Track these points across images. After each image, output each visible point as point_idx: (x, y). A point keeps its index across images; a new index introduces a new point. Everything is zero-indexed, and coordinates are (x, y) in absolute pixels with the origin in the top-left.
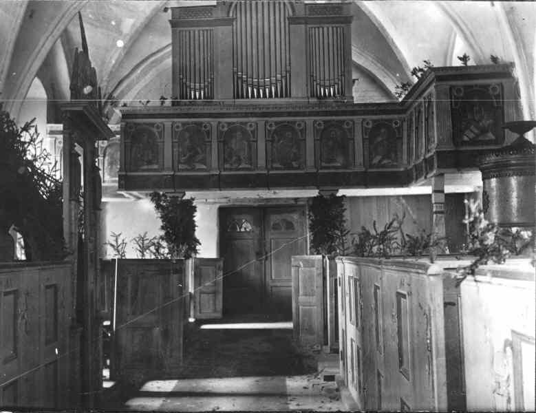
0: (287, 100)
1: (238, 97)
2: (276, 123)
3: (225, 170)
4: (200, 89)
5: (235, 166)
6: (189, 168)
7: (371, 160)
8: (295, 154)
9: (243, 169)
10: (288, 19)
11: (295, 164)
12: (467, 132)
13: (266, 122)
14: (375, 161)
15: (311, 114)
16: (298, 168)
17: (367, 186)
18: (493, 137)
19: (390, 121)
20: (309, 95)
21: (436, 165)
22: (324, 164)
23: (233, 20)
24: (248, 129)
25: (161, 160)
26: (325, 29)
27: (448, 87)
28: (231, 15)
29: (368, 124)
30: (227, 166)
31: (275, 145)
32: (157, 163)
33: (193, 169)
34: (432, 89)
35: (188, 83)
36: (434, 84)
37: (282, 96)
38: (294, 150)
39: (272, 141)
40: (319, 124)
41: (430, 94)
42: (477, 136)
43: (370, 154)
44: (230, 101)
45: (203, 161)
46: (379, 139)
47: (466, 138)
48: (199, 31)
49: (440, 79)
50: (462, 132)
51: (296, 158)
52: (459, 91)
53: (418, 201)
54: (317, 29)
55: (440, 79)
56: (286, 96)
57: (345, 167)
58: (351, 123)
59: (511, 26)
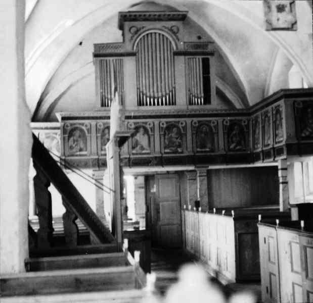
0: (174, 106)
3: (133, 154)
5: (139, 151)
8: (179, 143)
11: (179, 150)
12: (305, 131)
13: (128, 123)
14: (232, 146)
15: (189, 116)
16: (182, 153)
19: (210, 121)
22: (199, 150)
25: (89, 148)
26: (197, 60)
28: (135, 48)
30: (134, 152)
31: (167, 137)
32: (86, 150)
39: (165, 135)
43: (228, 141)
44: (136, 108)
46: (234, 132)
47: (303, 135)
50: (302, 131)
51: (180, 146)
52: (299, 104)
56: (173, 104)
57: (212, 151)
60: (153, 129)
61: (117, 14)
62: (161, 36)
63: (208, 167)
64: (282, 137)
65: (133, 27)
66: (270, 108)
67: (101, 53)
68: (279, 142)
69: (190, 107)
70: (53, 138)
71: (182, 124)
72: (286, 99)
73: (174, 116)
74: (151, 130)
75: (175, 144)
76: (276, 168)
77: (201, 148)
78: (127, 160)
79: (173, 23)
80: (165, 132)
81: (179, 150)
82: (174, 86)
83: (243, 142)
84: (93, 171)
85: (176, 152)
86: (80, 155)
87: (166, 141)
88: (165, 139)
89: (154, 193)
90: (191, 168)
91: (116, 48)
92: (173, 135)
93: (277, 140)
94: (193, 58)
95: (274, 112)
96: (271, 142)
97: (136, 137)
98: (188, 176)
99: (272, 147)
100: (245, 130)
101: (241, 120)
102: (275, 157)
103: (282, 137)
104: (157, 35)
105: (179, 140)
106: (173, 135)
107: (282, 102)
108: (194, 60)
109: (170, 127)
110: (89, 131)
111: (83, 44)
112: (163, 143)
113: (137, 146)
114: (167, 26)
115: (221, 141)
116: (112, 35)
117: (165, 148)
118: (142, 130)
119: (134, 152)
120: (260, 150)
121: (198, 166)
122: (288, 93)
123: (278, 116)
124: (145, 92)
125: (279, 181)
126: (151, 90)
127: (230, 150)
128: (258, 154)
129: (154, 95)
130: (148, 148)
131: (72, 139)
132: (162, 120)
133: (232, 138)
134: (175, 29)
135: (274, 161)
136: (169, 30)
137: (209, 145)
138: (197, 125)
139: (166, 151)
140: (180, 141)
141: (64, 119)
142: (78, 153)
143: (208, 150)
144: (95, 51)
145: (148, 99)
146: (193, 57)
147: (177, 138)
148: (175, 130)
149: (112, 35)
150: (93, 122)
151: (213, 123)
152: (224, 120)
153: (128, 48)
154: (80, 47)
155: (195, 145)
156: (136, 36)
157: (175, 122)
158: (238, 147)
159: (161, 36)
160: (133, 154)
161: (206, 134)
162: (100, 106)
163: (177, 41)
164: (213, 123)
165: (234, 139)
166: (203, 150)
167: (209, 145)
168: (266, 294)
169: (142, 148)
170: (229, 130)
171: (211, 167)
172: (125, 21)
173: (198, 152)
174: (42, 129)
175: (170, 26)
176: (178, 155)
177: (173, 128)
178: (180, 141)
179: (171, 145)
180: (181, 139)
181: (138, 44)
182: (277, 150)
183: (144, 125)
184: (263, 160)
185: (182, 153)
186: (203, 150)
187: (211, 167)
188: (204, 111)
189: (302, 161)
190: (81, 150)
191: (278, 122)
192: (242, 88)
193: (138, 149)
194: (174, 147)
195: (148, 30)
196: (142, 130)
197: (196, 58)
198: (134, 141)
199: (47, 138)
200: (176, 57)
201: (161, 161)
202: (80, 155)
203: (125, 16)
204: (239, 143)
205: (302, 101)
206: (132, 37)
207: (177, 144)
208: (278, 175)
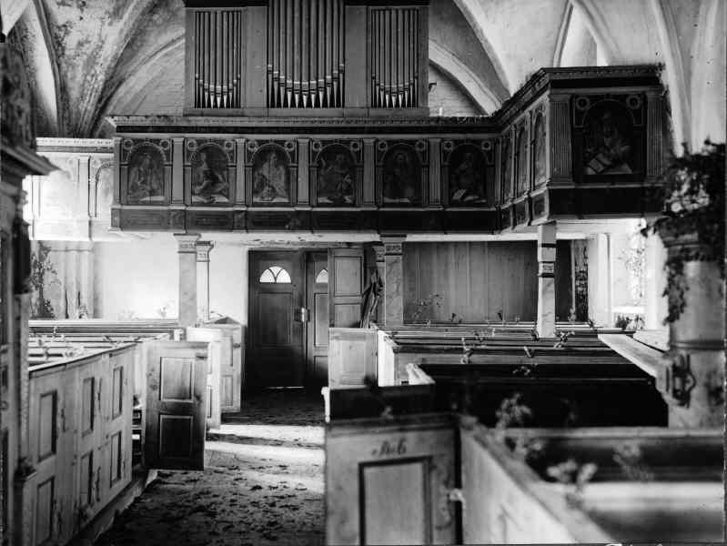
1: (273, 106)
2: (324, 142)
3: (255, 205)
4: (222, 93)
11: (348, 199)
12: (593, 162)
14: (457, 196)
15: (371, 131)
16: (353, 205)
17: (445, 231)
20: (370, 105)
22: (387, 200)
27: (569, 97)
34: (545, 98)
35: (206, 84)
36: (548, 92)
37: (332, 106)
40: (382, 146)
42: (608, 168)
45: (225, 193)
46: (463, 166)
47: (590, 171)
48: (222, 12)
49: (556, 85)
50: (586, 164)
51: (349, 191)
52: (583, 103)
55: (556, 85)
56: (338, 106)
64: (544, 174)
66: (526, 113)
69: (373, 112)
71: (355, 146)
72: (553, 91)
74: (232, 158)
77: (391, 198)
78: (243, 214)
80: (319, 162)
81: (348, 199)
83: (481, 189)
84: (381, 236)
89: (323, 286)
90: (375, 237)
94: (384, 11)
99: (526, 196)
102: (531, 219)
105: (347, 179)
108: (387, 13)
109: (330, 151)
110: (169, 154)
112: (314, 183)
115: (435, 180)
117: (319, 194)
119: (257, 200)
122: (558, 77)
123: (540, 129)
126: (394, 80)
128: (506, 212)
129: (215, 89)
130: (284, 193)
131: (135, 169)
132: (379, 136)
133: (457, 178)
137: (410, 191)
138: (386, 149)
139: (321, 200)
140: (349, 181)
141: (121, 129)
142: (148, 199)
143: (406, 200)
145: (289, 94)
146: (384, 7)
147: (344, 175)
151: (289, 146)
157: (341, 141)
158: (470, 198)
165: (463, 181)
174: (97, 150)
178: (349, 181)
184: (515, 225)
186: (397, 201)
188: (410, 121)
190: (152, 193)
191: (539, 144)
197: (390, 10)
202: (151, 203)
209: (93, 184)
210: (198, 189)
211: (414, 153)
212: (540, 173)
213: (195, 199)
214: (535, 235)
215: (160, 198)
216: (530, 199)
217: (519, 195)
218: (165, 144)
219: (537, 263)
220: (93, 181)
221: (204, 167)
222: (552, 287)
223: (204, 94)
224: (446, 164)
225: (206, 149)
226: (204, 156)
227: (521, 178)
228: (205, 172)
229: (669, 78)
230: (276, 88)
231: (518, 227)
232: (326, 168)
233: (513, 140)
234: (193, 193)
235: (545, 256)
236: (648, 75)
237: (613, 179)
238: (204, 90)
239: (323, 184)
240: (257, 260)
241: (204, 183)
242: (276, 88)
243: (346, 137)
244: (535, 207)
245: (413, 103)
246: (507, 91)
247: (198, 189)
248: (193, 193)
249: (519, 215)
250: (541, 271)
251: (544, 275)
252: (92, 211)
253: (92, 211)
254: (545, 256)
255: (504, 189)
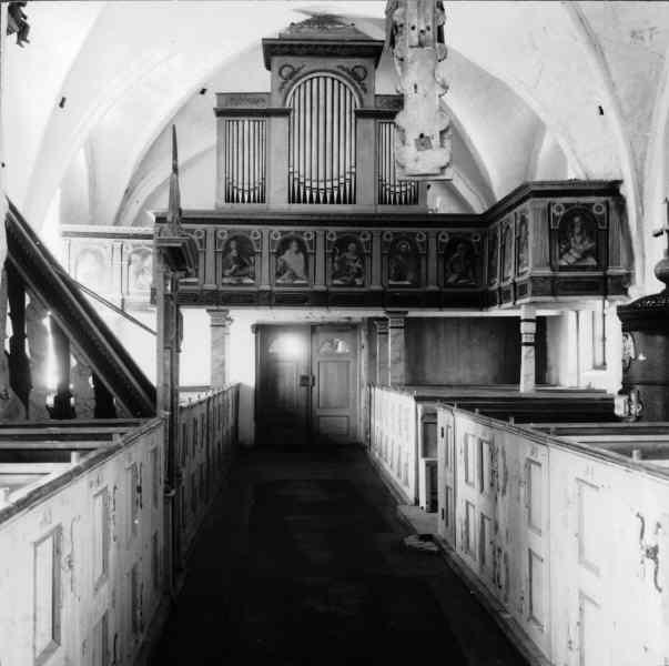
1: (293, 202)
3: (278, 285)
5: (289, 281)
6: (234, 282)
7: (446, 279)
8: (359, 269)
9: (301, 285)
10: (356, 112)
11: (358, 282)
13: (326, 232)
14: (451, 280)
16: (363, 286)
17: (441, 307)
18: (595, 263)
19: (414, 235)
21: (529, 292)
22: (391, 282)
23: (290, 110)
24: (305, 239)
25: (201, 272)
29: (443, 237)
32: (197, 276)
33: (242, 284)
38: (357, 265)
39: (333, 255)
41: (508, 220)
42: (578, 260)
43: (446, 271)
46: (456, 255)
51: (359, 274)
53: (458, 325)
54: (322, 80)
56: (350, 203)
57: (416, 284)
58: (369, 236)
59: (466, 149)
60: (313, 244)
61: (261, 42)
62: (336, 83)
63: (406, 312)
64: (527, 265)
65: (290, 66)
67: (233, 109)
68: (523, 274)
70: (145, 256)
71: (255, 235)
73: (352, 224)
74: (201, 244)
75: (351, 271)
76: (517, 320)
79: (358, 61)
81: (358, 282)
82: (353, 170)
83: (471, 274)
85: (353, 284)
86: (186, 284)
87: (336, 265)
88: (333, 261)
90: (380, 313)
91: (256, 102)
92: (348, 255)
93: (520, 271)
95: (518, 221)
96: (511, 273)
97: (283, 257)
98: (378, 326)
100: (476, 252)
101: (249, 232)
103: (527, 265)
104: (329, 81)
105: (357, 265)
106: (348, 255)
107: (527, 205)
109: (342, 243)
111: (207, 93)
112: (329, 268)
113: (285, 272)
114: (346, 66)
116: (258, 80)
117: (334, 277)
118: (294, 246)
120: (496, 287)
121: (389, 309)
123: (524, 228)
124: (302, 180)
125: (520, 339)
127: (448, 285)
130: (304, 277)
134: (361, 73)
135: (516, 307)
136: (349, 73)
137: (411, 276)
139: (336, 282)
143: (407, 283)
144: (219, 105)
148: (352, 246)
149: (258, 80)
150: (210, 228)
151: (364, 236)
152: (271, 231)
153: (276, 104)
154: (200, 96)
155: (385, 273)
156: (291, 82)
159: (336, 83)
160: (278, 285)
161: (406, 255)
162: (223, 200)
163: (362, 92)
164: (308, 235)
166: (400, 283)
167: (411, 276)
168: (154, 510)
169: (294, 276)
170: (447, 251)
171: (414, 313)
172: (274, 54)
173: (391, 286)
174: (128, 236)
175: (353, 66)
176: (356, 289)
177: (349, 242)
179: (344, 272)
180: (363, 263)
181: (294, 93)
182: (520, 287)
183: (299, 236)
184: (501, 303)
185: (363, 286)
186: (400, 283)
187: (414, 313)
189: (576, 308)
191: (522, 240)
192: (483, 174)
193: (285, 279)
194: (349, 276)
195: (306, 75)
196: (294, 246)
197: (243, 121)
198: (280, 263)
199: (137, 252)
200: (360, 121)
201: (323, 300)
203: (273, 46)
204: (463, 275)
205: (564, 204)
206: (283, 84)
207: (355, 271)
208: (519, 330)
209: (125, 267)
210: (227, 272)
211: (469, 243)
212: (532, 261)
213: (225, 280)
214: (521, 313)
215: (195, 280)
216: (514, 284)
217: (504, 279)
218: (199, 234)
219: (520, 334)
220: (125, 263)
221: (234, 253)
222: (533, 354)
223: (305, 193)
224: (386, 252)
225: (235, 238)
226: (233, 244)
227: (506, 266)
228: (234, 258)
229: (627, 190)
230: (302, 191)
231: (504, 306)
232: (340, 254)
233: (499, 234)
234: (223, 276)
235: (527, 329)
236: (612, 189)
237: (584, 268)
238: (233, 187)
239: (337, 268)
240: (263, 331)
241: (234, 267)
242: (302, 191)
243: (356, 229)
244: (519, 290)
245: (415, 201)
246: (494, 199)
247: (227, 272)
248: (223, 276)
249: (502, 297)
250: (524, 340)
251: (527, 344)
252: (125, 290)
253: (125, 290)
254: (527, 329)
255: (492, 275)
